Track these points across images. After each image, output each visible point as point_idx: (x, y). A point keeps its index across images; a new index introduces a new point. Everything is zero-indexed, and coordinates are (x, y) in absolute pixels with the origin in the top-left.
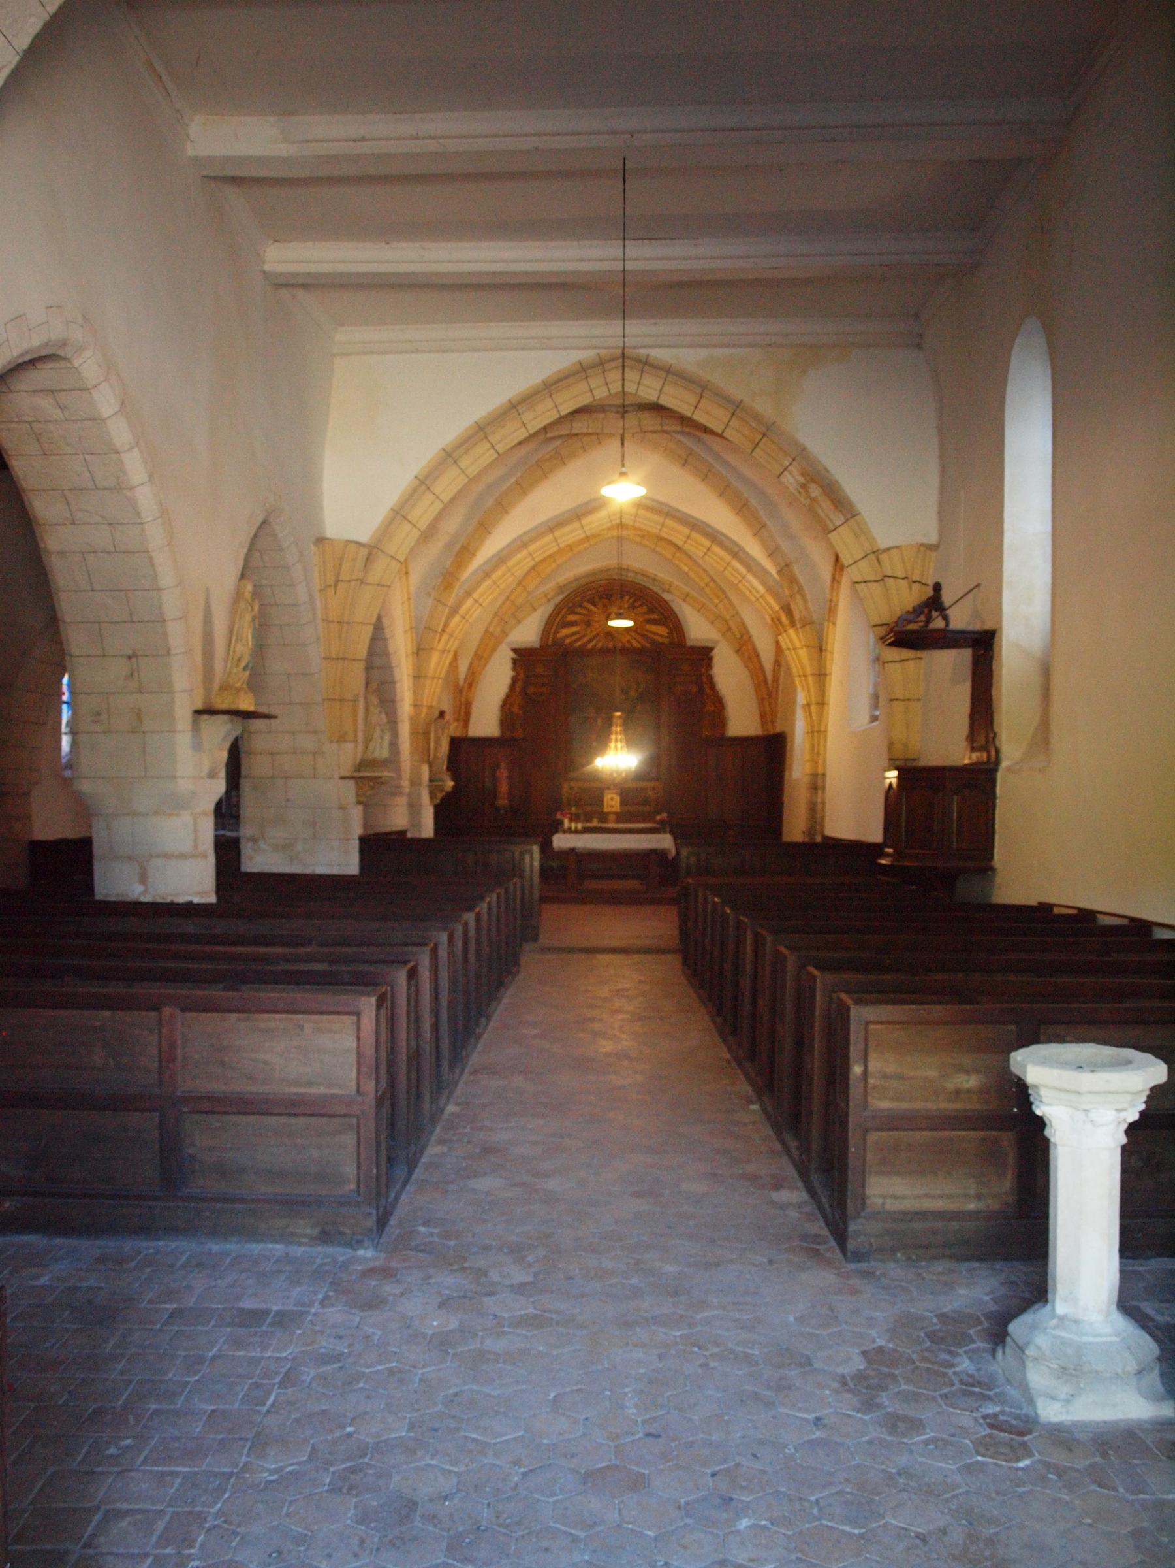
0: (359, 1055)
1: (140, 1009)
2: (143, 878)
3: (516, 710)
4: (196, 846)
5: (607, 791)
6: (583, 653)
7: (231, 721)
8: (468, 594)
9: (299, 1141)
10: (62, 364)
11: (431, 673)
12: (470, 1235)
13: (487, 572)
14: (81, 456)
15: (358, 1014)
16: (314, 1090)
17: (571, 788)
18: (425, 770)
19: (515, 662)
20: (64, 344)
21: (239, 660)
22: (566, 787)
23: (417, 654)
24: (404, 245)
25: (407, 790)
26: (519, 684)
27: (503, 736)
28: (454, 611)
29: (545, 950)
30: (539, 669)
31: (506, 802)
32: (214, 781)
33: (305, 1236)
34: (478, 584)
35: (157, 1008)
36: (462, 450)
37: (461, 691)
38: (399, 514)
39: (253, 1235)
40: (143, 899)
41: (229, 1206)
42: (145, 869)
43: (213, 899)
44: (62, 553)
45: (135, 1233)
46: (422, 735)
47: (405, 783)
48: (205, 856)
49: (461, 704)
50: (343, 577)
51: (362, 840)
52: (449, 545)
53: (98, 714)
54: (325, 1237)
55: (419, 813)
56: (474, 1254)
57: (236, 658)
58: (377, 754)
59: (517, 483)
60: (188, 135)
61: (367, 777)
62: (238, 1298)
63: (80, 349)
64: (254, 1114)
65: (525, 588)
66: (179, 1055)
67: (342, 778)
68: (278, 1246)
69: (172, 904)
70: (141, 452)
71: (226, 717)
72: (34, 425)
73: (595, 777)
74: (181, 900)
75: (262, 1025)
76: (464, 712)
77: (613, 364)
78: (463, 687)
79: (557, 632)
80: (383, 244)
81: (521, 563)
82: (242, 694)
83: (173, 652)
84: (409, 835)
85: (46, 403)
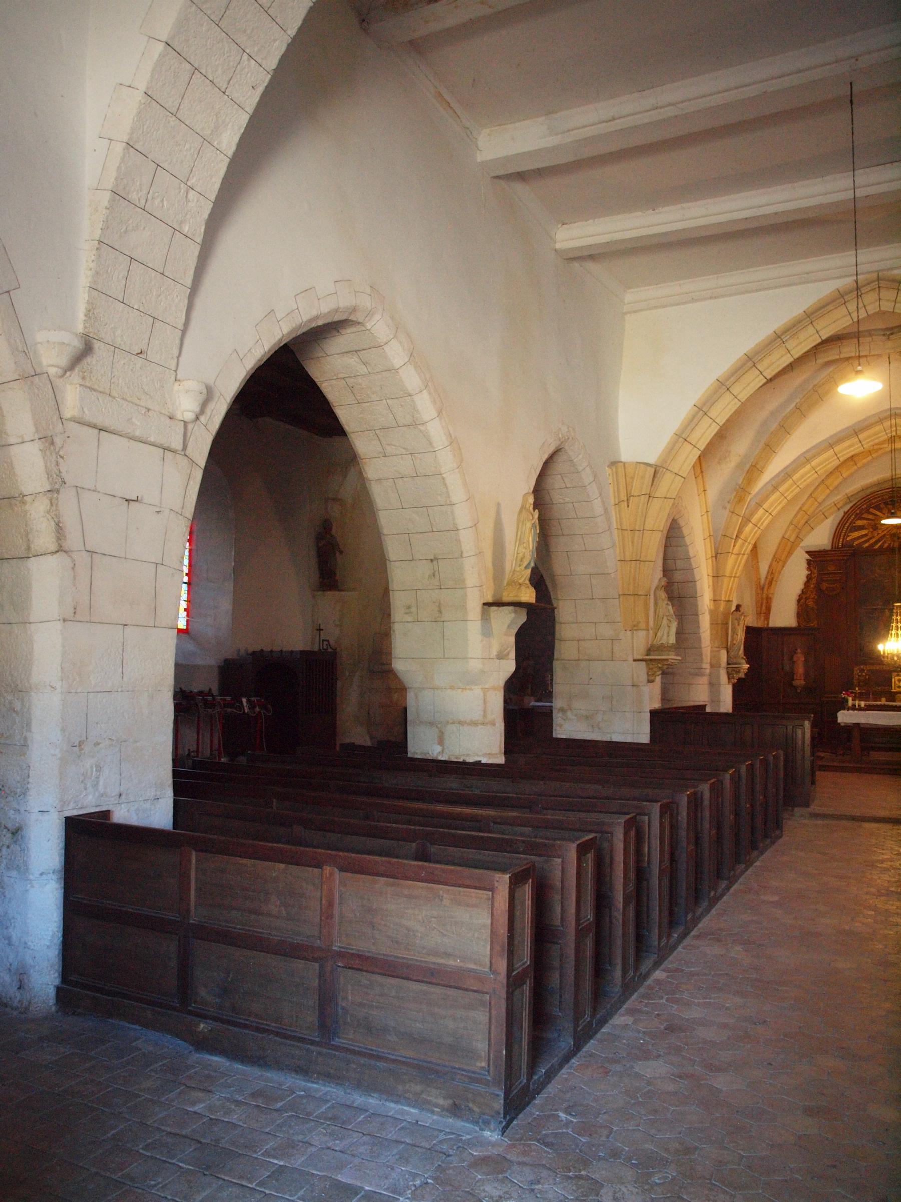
0: (493, 933)
1: (302, 866)
2: (441, 742)
3: (811, 603)
4: (484, 716)
5: (894, 674)
6: (871, 552)
7: (515, 612)
8: (759, 505)
9: (436, 1010)
10: (359, 328)
11: (728, 573)
12: (605, 1132)
13: (775, 485)
14: (385, 401)
15: (492, 889)
16: (451, 962)
17: (862, 670)
18: (724, 654)
19: (809, 563)
20: (354, 309)
21: (521, 561)
22: (856, 670)
23: (716, 557)
24: (666, 209)
25: (708, 671)
26: (814, 581)
27: (799, 625)
28: (747, 520)
29: (816, 816)
30: (831, 569)
31: (803, 682)
32: (503, 662)
33: (437, 1106)
34: (767, 497)
35: (319, 866)
36: (733, 379)
37: (763, 589)
38: (682, 437)
39: (390, 1094)
40: (440, 758)
41: (373, 1062)
42: (443, 733)
43: (500, 760)
44: (379, 480)
45: (296, 1071)
46: (721, 624)
47: (706, 666)
48: (493, 723)
49: (762, 599)
50: (635, 492)
51: (654, 714)
52: (739, 466)
53: (409, 607)
54: (455, 1110)
55: (719, 691)
56: (600, 1159)
57: (519, 559)
58: (664, 641)
59: (798, 408)
60: (477, 147)
61: (655, 659)
62: (340, 1167)
63: (370, 314)
64: (398, 977)
65: (816, 500)
66: (336, 911)
67: (634, 660)
68: (413, 1110)
69: (464, 763)
70: (430, 393)
71: (511, 608)
72: (347, 380)
73: (878, 659)
74: (470, 760)
75: (406, 892)
76: (765, 606)
77: (869, 288)
78: (764, 585)
79: (846, 535)
80: (651, 212)
81: (806, 476)
82: (523, 589)
83: (465, 555)
84: (708, 710)
85: (352, 361)
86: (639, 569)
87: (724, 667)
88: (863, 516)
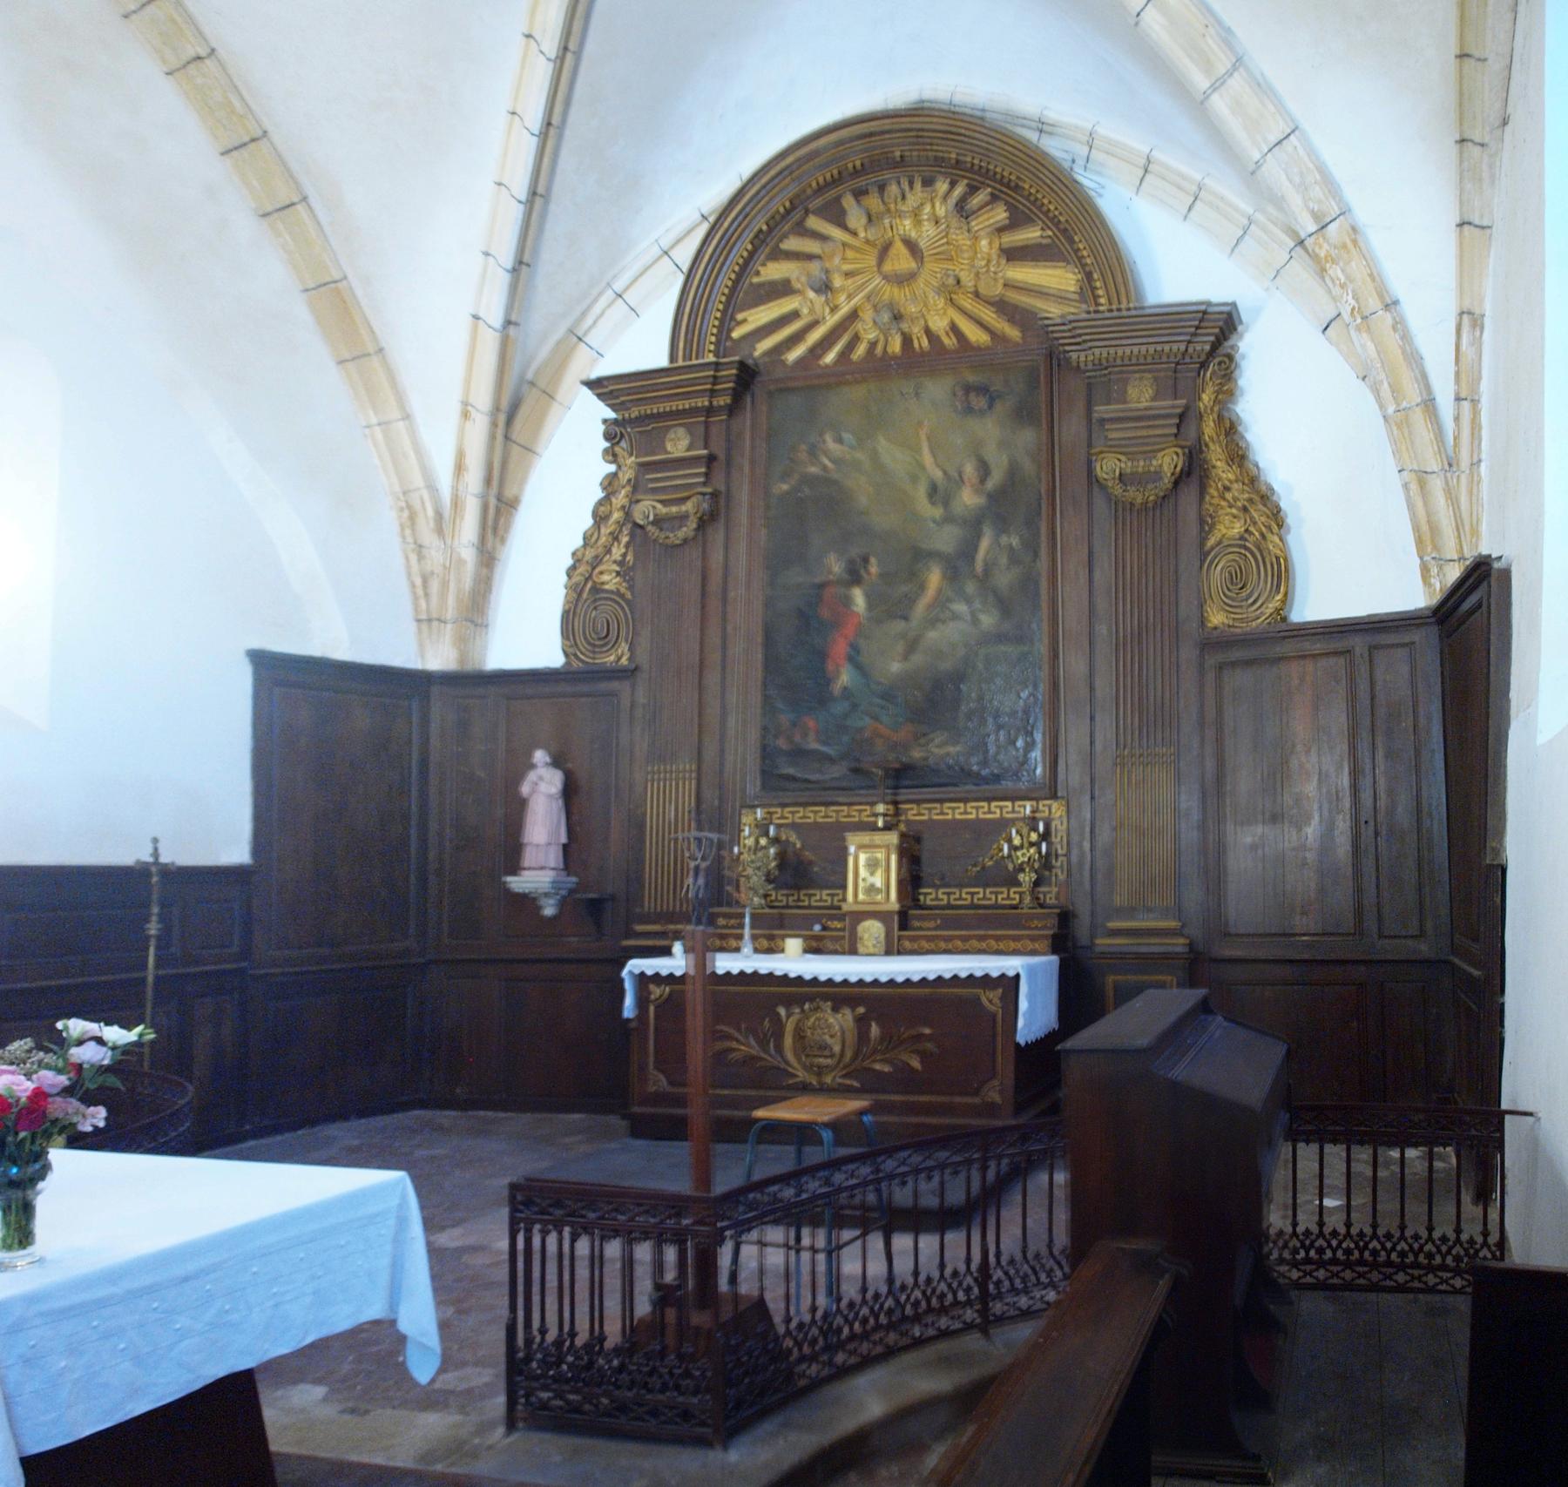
3: (610, 580)
79: (728, 320)
86: (420, 547)
87: (547, 764)
88: (785, 245)
